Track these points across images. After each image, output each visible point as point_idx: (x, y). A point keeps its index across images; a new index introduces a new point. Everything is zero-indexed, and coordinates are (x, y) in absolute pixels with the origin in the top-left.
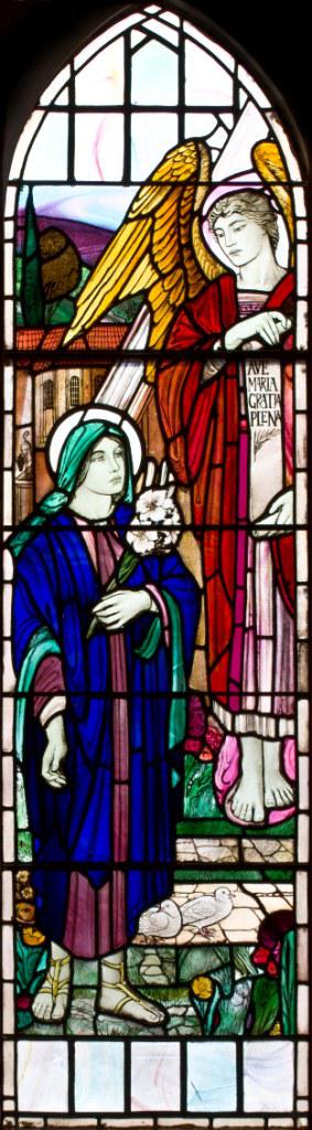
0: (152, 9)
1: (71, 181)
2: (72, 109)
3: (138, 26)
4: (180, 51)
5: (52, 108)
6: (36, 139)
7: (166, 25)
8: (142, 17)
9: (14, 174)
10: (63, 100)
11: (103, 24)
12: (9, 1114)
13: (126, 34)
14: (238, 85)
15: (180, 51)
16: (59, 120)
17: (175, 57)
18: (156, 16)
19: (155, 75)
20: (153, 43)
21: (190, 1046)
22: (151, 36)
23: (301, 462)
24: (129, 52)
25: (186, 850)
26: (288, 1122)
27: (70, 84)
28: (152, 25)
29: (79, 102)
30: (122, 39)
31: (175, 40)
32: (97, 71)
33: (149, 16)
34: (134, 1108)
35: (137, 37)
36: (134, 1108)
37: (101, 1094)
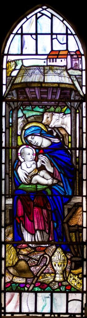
0: (44, 7)
1: (37, 54)
2: (22, 34)
3: (39, 12)
4: (52, 19)
5: (17, 34)
6: (75, 41)
7: (49, 12)
8: (41, 9)
9: (6, 52)
10: (20, 32)
11: (57, 11)
12: (3, 313)
13: (36, 14)
14: (67, 28)
15: (52, 19)
16: (18, 37)
17: (50, 20)
18: (45, 9)
19: (44, 24)
20: (44, 16)
21: (38, 294)
22: (43, 14)
23: (84, 130)
24: (37, 19)
25: (34, 240)
26: (49, 315)
27: (21, 27)
28: (44, 12)
29: (34, 32)
30: (35, 16)
31: (50, 16)
32: (28, 25)
33: (43, 9)
34: (81, 300)
35: (39, 15)
36: (81, 300)
37: (28, 307)
